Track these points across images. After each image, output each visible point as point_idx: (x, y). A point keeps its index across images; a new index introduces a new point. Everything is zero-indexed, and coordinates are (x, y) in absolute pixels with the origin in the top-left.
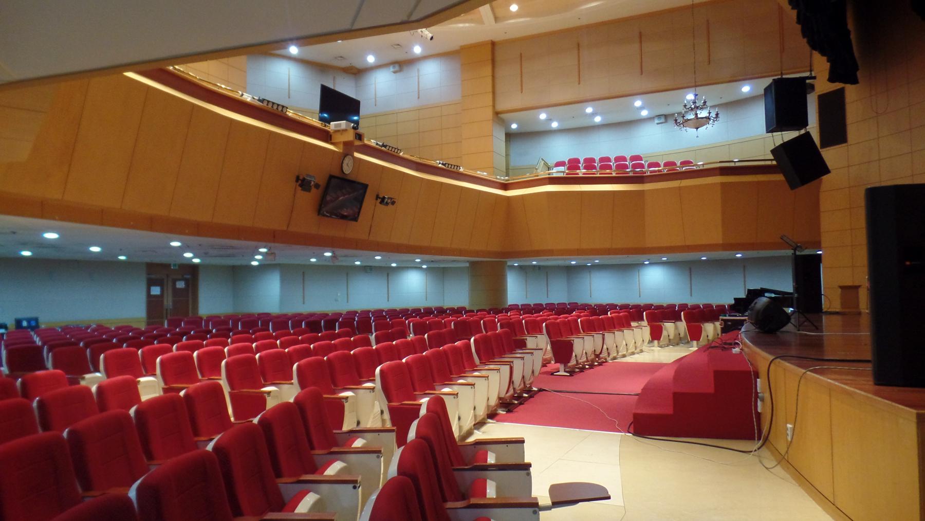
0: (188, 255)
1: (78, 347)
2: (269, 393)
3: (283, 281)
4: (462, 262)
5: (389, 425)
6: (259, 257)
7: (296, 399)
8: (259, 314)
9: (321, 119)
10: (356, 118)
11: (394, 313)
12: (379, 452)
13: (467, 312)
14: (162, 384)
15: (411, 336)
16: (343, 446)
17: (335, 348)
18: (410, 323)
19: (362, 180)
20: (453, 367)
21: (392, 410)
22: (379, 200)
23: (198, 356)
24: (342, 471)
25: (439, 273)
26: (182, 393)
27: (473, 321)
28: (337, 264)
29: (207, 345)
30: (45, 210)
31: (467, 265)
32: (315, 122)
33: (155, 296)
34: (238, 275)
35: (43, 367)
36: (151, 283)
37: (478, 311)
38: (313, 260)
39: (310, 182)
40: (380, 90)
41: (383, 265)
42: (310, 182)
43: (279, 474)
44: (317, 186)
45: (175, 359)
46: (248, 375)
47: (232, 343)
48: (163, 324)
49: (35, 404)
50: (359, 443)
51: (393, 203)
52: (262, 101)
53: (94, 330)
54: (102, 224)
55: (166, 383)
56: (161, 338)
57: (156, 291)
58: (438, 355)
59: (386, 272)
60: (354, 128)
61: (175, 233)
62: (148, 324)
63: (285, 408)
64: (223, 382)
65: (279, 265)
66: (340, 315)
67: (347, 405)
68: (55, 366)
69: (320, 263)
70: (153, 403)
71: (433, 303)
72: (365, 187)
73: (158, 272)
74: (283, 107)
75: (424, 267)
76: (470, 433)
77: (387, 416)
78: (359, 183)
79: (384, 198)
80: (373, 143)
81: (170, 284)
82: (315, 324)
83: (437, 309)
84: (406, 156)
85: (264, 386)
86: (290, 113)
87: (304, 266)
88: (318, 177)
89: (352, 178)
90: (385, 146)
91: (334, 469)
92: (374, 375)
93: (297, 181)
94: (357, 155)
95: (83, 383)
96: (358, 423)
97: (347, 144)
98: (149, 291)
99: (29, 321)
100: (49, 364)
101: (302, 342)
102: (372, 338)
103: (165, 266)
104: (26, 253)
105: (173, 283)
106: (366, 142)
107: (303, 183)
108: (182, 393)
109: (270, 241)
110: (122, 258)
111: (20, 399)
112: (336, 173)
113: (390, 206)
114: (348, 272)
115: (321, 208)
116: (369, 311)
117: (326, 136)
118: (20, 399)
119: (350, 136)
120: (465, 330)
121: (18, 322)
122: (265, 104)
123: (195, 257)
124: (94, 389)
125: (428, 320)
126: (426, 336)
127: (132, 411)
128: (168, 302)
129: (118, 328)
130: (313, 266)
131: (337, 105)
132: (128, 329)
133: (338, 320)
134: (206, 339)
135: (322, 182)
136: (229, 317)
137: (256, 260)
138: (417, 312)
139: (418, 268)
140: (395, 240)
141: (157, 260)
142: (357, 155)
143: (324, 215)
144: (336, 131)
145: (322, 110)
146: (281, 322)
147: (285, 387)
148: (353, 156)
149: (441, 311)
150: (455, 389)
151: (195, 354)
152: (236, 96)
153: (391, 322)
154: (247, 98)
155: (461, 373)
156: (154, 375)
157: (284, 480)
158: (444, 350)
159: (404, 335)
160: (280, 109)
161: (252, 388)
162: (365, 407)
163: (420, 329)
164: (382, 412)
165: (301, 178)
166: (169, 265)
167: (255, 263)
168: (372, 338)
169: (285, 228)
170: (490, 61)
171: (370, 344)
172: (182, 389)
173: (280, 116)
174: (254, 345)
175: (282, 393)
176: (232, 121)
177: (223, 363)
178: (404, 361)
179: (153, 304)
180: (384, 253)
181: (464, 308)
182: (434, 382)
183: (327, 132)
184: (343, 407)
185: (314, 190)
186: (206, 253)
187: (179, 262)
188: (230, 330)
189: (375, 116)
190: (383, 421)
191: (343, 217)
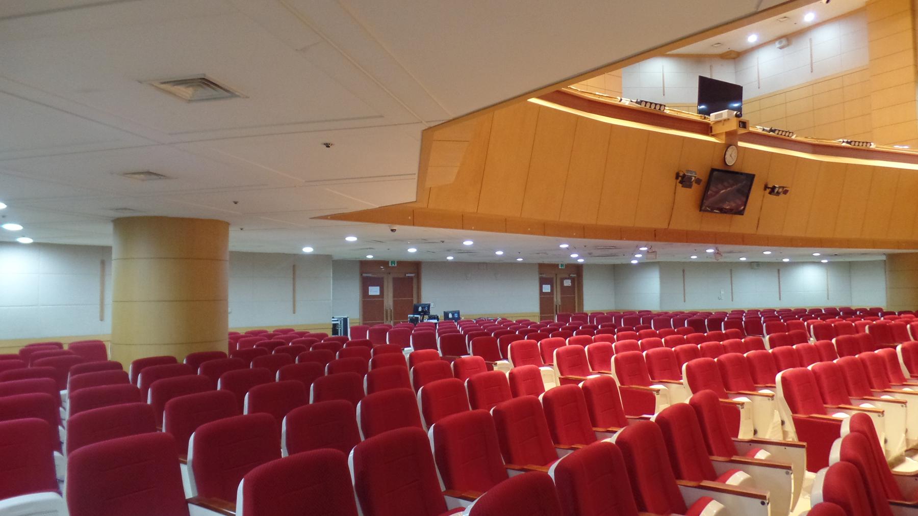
0: (574, 256)
1: (492, 338)
2: (658, 391)
3: (661, 278)
5: (792, 437)
7: (691, 400)
8: (640, 312)
9: (700, 112)
10: (736, 105)
11: (788, 314)
12: (789, 468)
13: (884, 314)
14: (559, 375)
15: (812, 341)
16: (744, 455)
17: (724, 349)
18: (810, 326)
20: (875, 379)
21: (798, 423)
22: (768, 190)
25: (846, 269)
26: (580, 385)
27: (895, 325)
29: (595, 341)
30: (463, 222)
31: (884, 258)
32: (695, 116)
34: (618, 273)
37: (900, 313)
39: (690, 178)
40: (767, 69)
41: (774, 260)
42: (690, 178)
43: (679, 477)
44: (698, 181)
45: (569, 353)
49: (466, 384)
51: (786, 192)
52: (640, 103)
55: (562, 374)
56: (554, 331)
58: (854, 364)
59: (778, 268)
60: (737, 116)
62: (541, 319)
69: (701, 260)
70: (555, 393)
71: (838, 302)
72: (751, 178)
73: (548, 272)
75: (825, 261)
76: (900, 460)
77: (790, 428)
78: (742, 174)
79: (774, 187)
80: (758, 129)
82: (698, 323)
83: (841, 309)
84: (799, 139)
86: (667, 111)
88: (698, 169)
89: (736, 169)
90: (774, 131)
91: (737, 479)
92: (774, 383)
94: (741, 144)
95: (496, 368)
96: (755, 432)
97: (730, 135)
100: (470, 351)
101: (688, 341)
102: (766, 339)
103: (555, 266)
104: (450, 258)
105: (562, 279)
106: (751, 129)
107: (684, 180)
108: (580, 385)
112: (718, 165)
113: (782, 196)
114: (733, 268)
115: (705, 204)
116: (758, 311)
117: (706, 129)
119: (733, 125)
120: (886, 334)
121: (446, 314)
122: (643, 105)
124: (507, 375)
125: (833, 322)
126: (834, 341)
127: (541, 398)
128: (557, 299)
129: (519, 322)
131: (716, 94)
133: (723, 320)
134: (593, 334)
135: (703, 174)
136: (612, 314)
137: (636, 259)
138: (816, 312)
139: (816, 263)
140: (789, 233)
141: (546, 261)
142: (741, 144)
143: (706, 211)
144: (717, 122)
145: (700, 103)
146: (663, 320)
147: (674, 387)
148: (737, 146)
149: (849, 313)
150: (879, 406)
151: (586, 349)
153: (787, 323)
154: (626, 102)
155: (885, 386)
158: (863, 361)
159: (805, 339)
160: (658, 107)
162: (765, 415)
163: (823, 333)
164: (783, 423)
165: (681, 174)
166: (558, 265)
167: (634, 262)
168: (766, 339)
169: (665, 226)
170: (909, 13)
171: (763, 347)
172: (580, 381)
173: (658, 115)
174: (639, 342)
175: (672, 395)
179: (545, 300)
180: (774, 248)
181: (880, 310)
183: (708, 124)
184: (739, 413)
185: (694, 185)
186: (590, 254)
187: (567, 262)
189: (759, 99)
190: (785, 433)
191: (722, 211)
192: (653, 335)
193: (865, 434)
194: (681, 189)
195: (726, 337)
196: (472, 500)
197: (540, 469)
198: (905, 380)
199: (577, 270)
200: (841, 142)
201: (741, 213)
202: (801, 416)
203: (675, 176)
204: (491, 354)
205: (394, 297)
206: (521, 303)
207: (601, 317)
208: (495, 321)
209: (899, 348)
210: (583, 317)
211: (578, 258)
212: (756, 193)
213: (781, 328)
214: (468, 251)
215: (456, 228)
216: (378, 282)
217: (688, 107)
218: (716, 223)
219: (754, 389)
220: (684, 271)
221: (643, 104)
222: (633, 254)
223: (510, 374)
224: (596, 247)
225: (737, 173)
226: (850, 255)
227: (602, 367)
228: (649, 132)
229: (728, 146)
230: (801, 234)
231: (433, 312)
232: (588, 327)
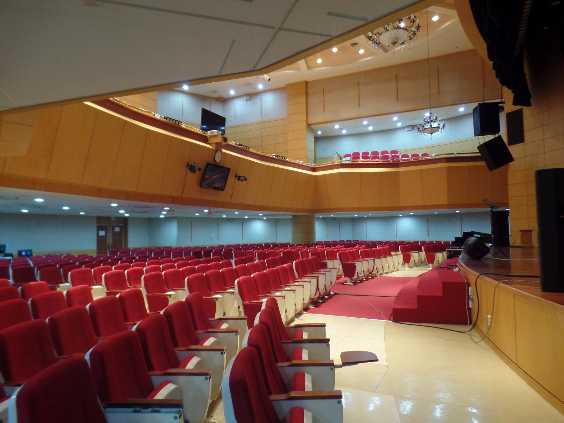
0: (122, 212)
1: (55, 268)
2: (170, 295)
3: (179, 227)
5: (243, 315)
6: (164, 213)
7: (186, 299)
8: (165, 247)
9: (202, 129)
10: (223, 128)
11: (246, 247)
12: (237, 332)
13: (290, 246)
14: (106, 290)
17: (210, 268)
18: (256, 253)
19: (227, 166)
20: (282, 280)
21: (245, 306)
22: (237, 178)
23: (128, 273)
25: (274, 222)
26: (118, 296)
29: (133, 266)
31: (291, 217)
32: (198, 131)
34: (152, 224)
35: (36, 280)
36: (99, 228)
37: (297, 245)
38: (197, 214)
39: (195, 167)
40: (238, 111)
42: (195, 167)
43: (176, 345)
44: (199, 169)
45: (114, 275)
47: (148, 265)
48: (106, 253)
49: (29, 302)
50: (224, 326)
51: (246, 180)
52: (166, 118)
53: (65, 257)
56: (105, 262)
57: (102, 233)
59: (242, 222)
60: (222, 134)
61: (236, 209)
62: (98, 253)
64: (143, 289)
67: (217, 303)
68: (42, 279)
70: (100, 301)
71: (270, 241)
73: (103, 222)
74: (179, 122)
75: (265, 218)
76: (292, 320)
77: (242, 309)
79: (240, 177)
80: (233, 143)
81: (111, 228)
82: (198, 253)
83: (272, 244)
84: (254, 151)
85: (167, 291)
86: (183, 126)
88: (200, 163)
89: (221, 164)
90: (241, 145)
91: (209, 342)
92: (234, 285)
94: (224, 151)
96: (224, 314)
97: (218, 144)
99: (26, 251)
100: (38, 278)
101: (190, 264)
102: (233, 262)
103: (108, 218)
104: (25, 211)
105: (113, 229)
106: (229, 143)
107: (191, 168)
108: (118, 296)
110: (82, 213)
112: (211, 162)
113: (244, 182)
114: (219, 221)
115: (203, 183)
116: (231, 246)
117: (205, 139)
119: (219, 139)
120: (289, 257)
121: (20, 253)
122: (168, 120)
124: (65, 293)
125: (267, 251)
126: (266, 261)
127: (88, 307)
128: (110, 240)
129: (79, 256)
131: (212, 120)
132: (86, 256)
135: (202, 166)
136: (146, 249)
137: (163, 214)
138: (260, 246)
139: (261, 219)
140: (248, 202)
141: (102, 215)
142: (224, 151)
144: (211, 136)
145: (203, 123)
146: (178, 252)
147: (180, 292)
148: (221, 151)
149: (275, 245)
150: (283, 293)
151: (126, 272)
152: (151, 115)
153: (244, 252)
154: (158, 116)
155: (287, 283)
156: (101, 284)
159: (252, 260)
160: (177, 123)
162: (228, 303)
164: (239, 307)
165: (190, 164)
166: (110, 218)
167: (162, 216)
168: (233, 262)
170: (305, 94)
174: (161, 266)
175: (178, 296)
179: (101, 241)
180: (240, 210)
181: (289, 244)
183: (206, 137)
185: (197, 172)
186: (132, 211)
188: (147, 257)
189: (235, 127)
190: (240, 313)
191: (215, 188)
192: (171, 261)
193: (273, 306)
194: (190, 175)
195: (212, 260)
196: (19, 385)
197: (77, 355)
198: (296, 279)
199: (124, 221)
200: (273, 156)
201: (222, 189)
202: (246, 302)
203: (186, 165)
204: (55, 278)
206: (84, 243)
207: (139, 251)
208: (61, 256)
209: (294, 263)
210: (127, 252)
211: (125, 213)
212: (231, 178)
213: (242, 255)
214: (39, 205)
215: (30, 188)
217: (195, 125)
218: (210, 195)
219: (225, 290)
220: (191, 222)
221: (168, 119)
222: (161, 212)
223: (68, 292)
224: (136, 207)
225: (222, 167)
226: (277, 215)
227: (136, 284)
229: (216, 151)
230: (253, 203)
231: (8, 251)
232: (130, 258)
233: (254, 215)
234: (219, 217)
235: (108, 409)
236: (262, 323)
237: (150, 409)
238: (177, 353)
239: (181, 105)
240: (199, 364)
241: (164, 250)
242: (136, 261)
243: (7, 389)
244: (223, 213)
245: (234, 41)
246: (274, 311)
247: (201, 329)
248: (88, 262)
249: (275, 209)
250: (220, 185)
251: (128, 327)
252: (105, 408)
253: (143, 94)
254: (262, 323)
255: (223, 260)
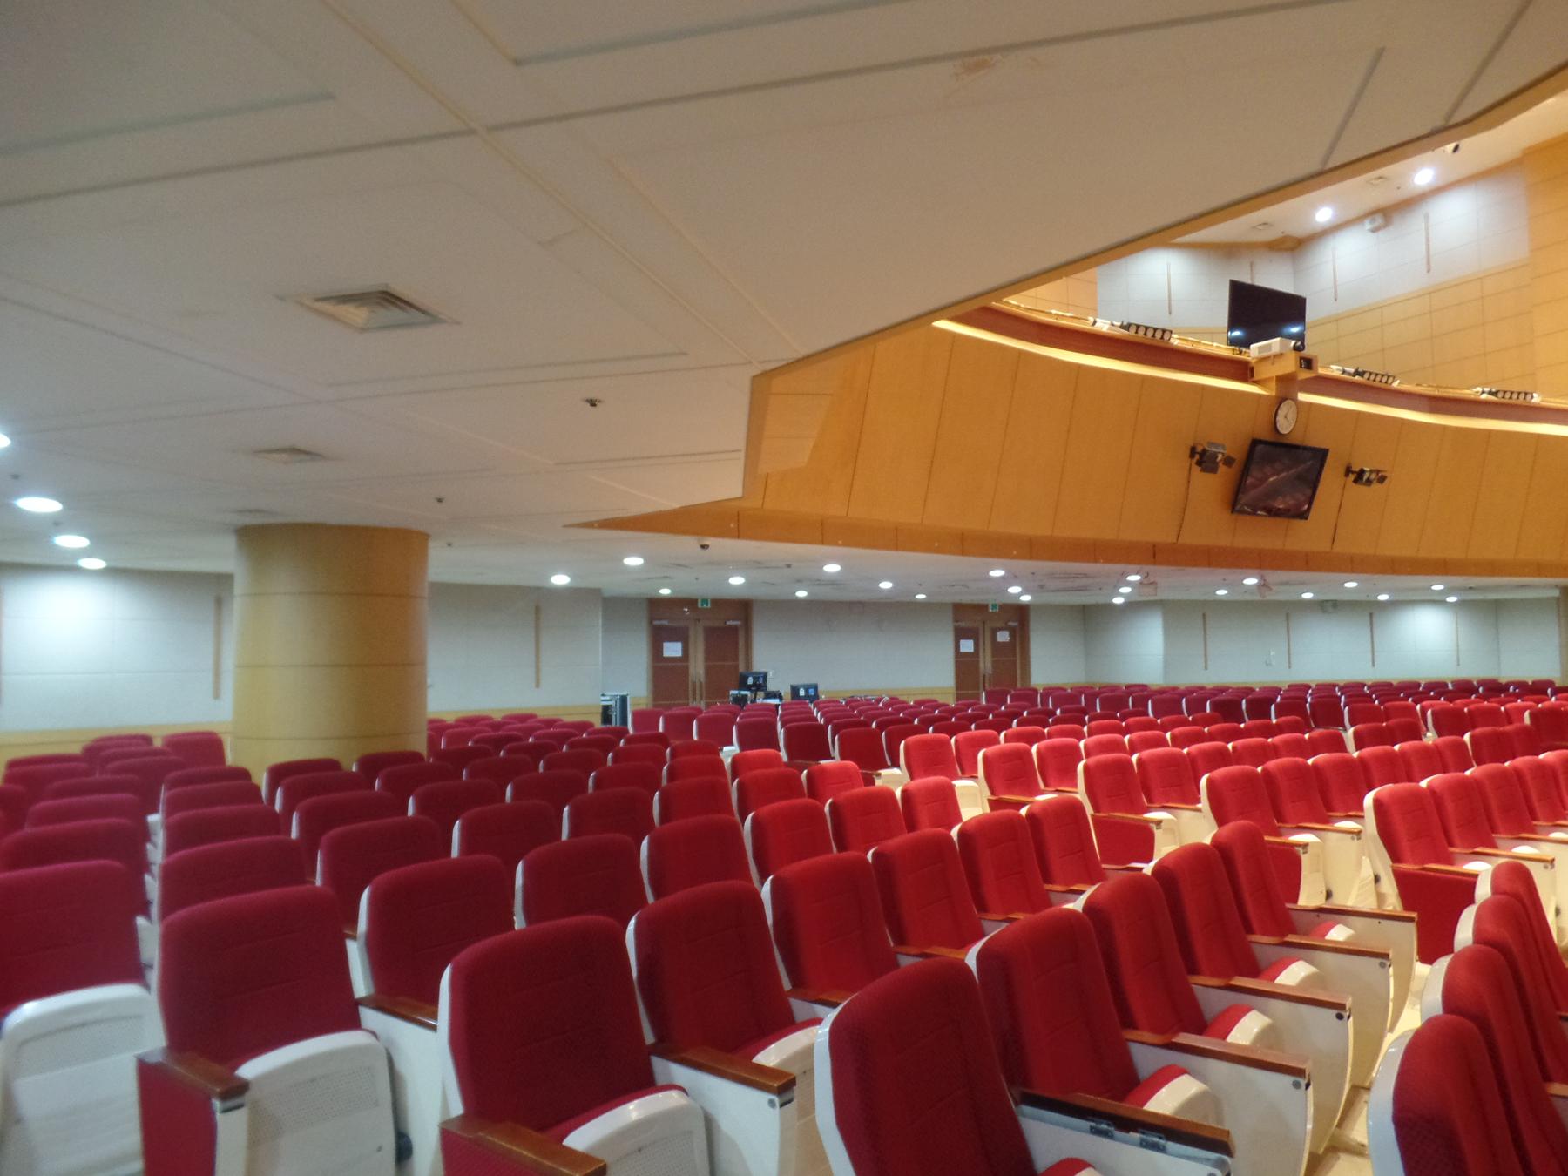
0: (1014, 590)
1: (872, 730)
2: (1159, 823)
4: (1545, 588)
5: (1393, 903)
6: (1125, 590)
7: (1214, 839)
8: (1128, 687)
9: (1233, 342)
10: (1295, 330)
11: (1387, 691)
14: (987, 793)
15: (1430, 737)
16: (1306, 934)
17: (1275, 752)
19: (1315, 441)
21: (1402, 879)
22: (1352, 477)
23: (1039, 752)
24: (1308, 981)
25: (1488, 612)
26: (1023, 811)
28: (1270, 597)
29: (1050, 736)
30: (824, 532)
31: (1556, 593)
32: (1221, 349)
33: (967, 654)
34: (1092, 620)
35: (829, 757)
36: (960, 634)
38: (1221, 592)
39: (1215, 455)
40: (1350, 267)
41: (1362, 597)
42: (1215, 455)
44: (1229, 461)
45: (1006, 756)
46: (1117, 785)
47: (1090, 734)
48: (979, 699)
49: (827, 809)
50: (1339, 933)
51: (1382, 479)
52: (1127, 327)
53: (887, 705)
54: (897, 548)
55: (993, 793)
56: (979, 719)
57: (967, 646)
59: (1369, 611)
60: (1296, 348)
61: (1353, 571)
62: (958, 698)
63: (1196, 855)
64: (1080, 794)
65: (1161, 604)
66: (1277, 690)
67: (1306, 860)
68: (843, 757)
70: (981, 824)
71: (1475, 670)
72: (1321, 455)
73: (970, 618)
74: (1164, 331)
75: (1452, 599)
77: (1390, 887)
78: (1305, 448)
79: (1362, 472)
80: (1335, 371)
81: (988, 635)
82: (1229, 706)
83: (1482, 683)
85: (1148, 810)
86: (1175, 341)
87: (1205, 603)
88: (1229, 440)
89: (1296, 439)
90: (1362, 374)
91: (1294, 975)
92: (1361, 808)
93: (1347, 475)
94: (1303, 397)
95: (879, 782)
96: (1329, 895)
98: (957, 646)
99: (807, 688)
100: (836, 752)
101: (1211, 737)
102: (1349, 735)
103: (981, 608)
104: (801, 594)
105: (992, 631)
106: (1321, 371)
107: (1204, 459)
108: (1023, 811)
109: (1148, 563)
110: (921, 597)
111: (806, 800)
112: (1264, 434)
113: (1376, 486)
114: (1290, 611)
115: (1238, 502)
116: (1334, 686)
117: (1243, 371)
118: (806, 800)
119: (1289, 365)
121: (795, 690)
123: (1024, 592)
124: (898, 793)
125: (1466, 706)
126: (1467, 737)
127: (954, 832)
128: (986, 664)
129: (919, 703)
130: (1221, 603)
131: (1260, 311)
132: (934, 705)
133: (1274, 701)
136: (1080, 690)
138: (1438, 688)
139: (1438, 602)
140: (1391, 547)
141: (967, 599)
144: (1262, 360)
145: (1232, 325)
146: (1169, 701)
147: (1186, 815)
148: (1295, 400)
149: (1494, 689)
150: (1545, 850)
151: (1034, 749)
152: (1085, 325)
153: (1386, 707)
154: (1103, 326)
156: (974, 778)
157: (990, 916)
159: (1416, 734)
160: (1158, 335)
161: (1127, 811)
162: (1345, 865)
163: (1449, 723)
164: (1377, 879)
165: (1199, 449)
166: (985, 607)
167: (1118, 600)
168: (1349, 735)
169: (1171, 539)
172: (1023, 804)
174: (1126, 739)
175: (1183, 829)
176: (1204, 387)
177: (1080, 767)
178: (1310, 762)
179: (965, 667)
181: (1550, 683)
182: (1494, 830)
185: (1222, 468)
186: (1042, 587)
188: (1084, 712)
189: (1336, 320)
190: (1381, 897)
191: (1273, 512)
192: (1151, 726)
195: (1279, 730)
196: (834, 1005)
200: (1480, 393)
201: (1303, 516)
202: (1406, 867)
203: (1188, 452)
204: (871, 757)
205: (707, 659)
206: (923, 670)
208: (878, 701)
210: (1029, 695)
212: (1331, 480)
213: (1374, 715)
214: (833, 582)
216: (679, 635)
217: (1211, 334)
220: (537, 609)
223: (904, 792)
224: (1052, 576)
225: (1296, 447)
226: (1497, 588)
228: (1358, 413)
229: (1281, 400)
230: (1407, 552)
231: (771, 687)
232: (1039, 712)
233: (1415, 589)
234: (1293, 597)
235: (1027, 1109)
236: (1486, 943)
237: (1136, 1136)
238: (1198, 990)
239: (1170, 288)
240: (1265, 1035)
241: (1130, 694)
242: (1056, 722)
243: (800, 1008)
244: (1305, 585)
245: (1383, 49)
246: (1524, 906)
247: (1264, 934)
248: (939, 719)
249: (1493, 568)
250: (1291, 502)
251: (1054, 897)
252: (1017, 1104)
253: (1079, 275)
254: (1486, 943)
255: (1310, 730)
